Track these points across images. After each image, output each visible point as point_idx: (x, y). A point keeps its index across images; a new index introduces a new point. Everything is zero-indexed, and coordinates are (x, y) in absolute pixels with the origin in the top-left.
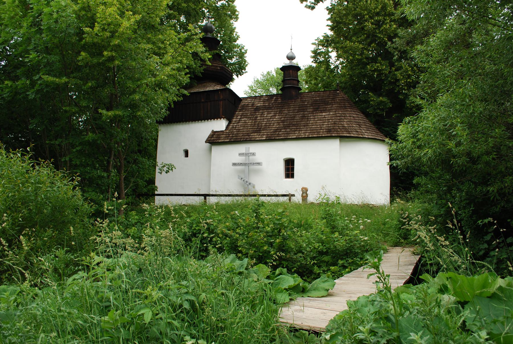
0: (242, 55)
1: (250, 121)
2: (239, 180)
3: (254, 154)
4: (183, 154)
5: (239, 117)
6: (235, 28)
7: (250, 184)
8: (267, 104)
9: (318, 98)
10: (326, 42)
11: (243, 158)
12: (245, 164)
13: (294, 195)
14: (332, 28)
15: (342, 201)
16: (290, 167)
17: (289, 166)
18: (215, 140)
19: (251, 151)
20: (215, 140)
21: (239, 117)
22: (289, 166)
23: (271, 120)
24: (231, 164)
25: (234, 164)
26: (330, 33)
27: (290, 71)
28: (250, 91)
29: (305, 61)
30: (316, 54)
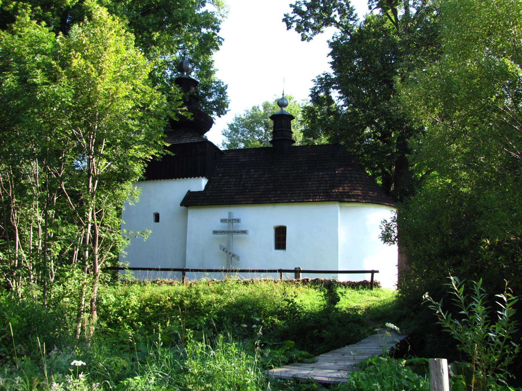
0: (222, 91)
1: (234, 180)
2: (221, 252)
3: (238, 221)
4: (152, 218)
5: (220, 175)
6: (213, 61)
7: (233, 256)
8: (254, 159)
9: (314, 154)
10: (325, 83)
11: (226, 224)
12: (228, 232)
13: (377, 272)
14: (334, 65)
15: (397, 283)
16: (281, 235)
17: (280, 237)
18: (192, 200)
19: (235, 217)
20: (192, 200)
21: (220, 175)
22: (280, 237)
23: (259, 179)
24: (212, 232)
25: (215, 232)
26: (331, 72)
27: (281, 121)
28: (230, 131)
29: (300, 98)
30: (315, 96)
